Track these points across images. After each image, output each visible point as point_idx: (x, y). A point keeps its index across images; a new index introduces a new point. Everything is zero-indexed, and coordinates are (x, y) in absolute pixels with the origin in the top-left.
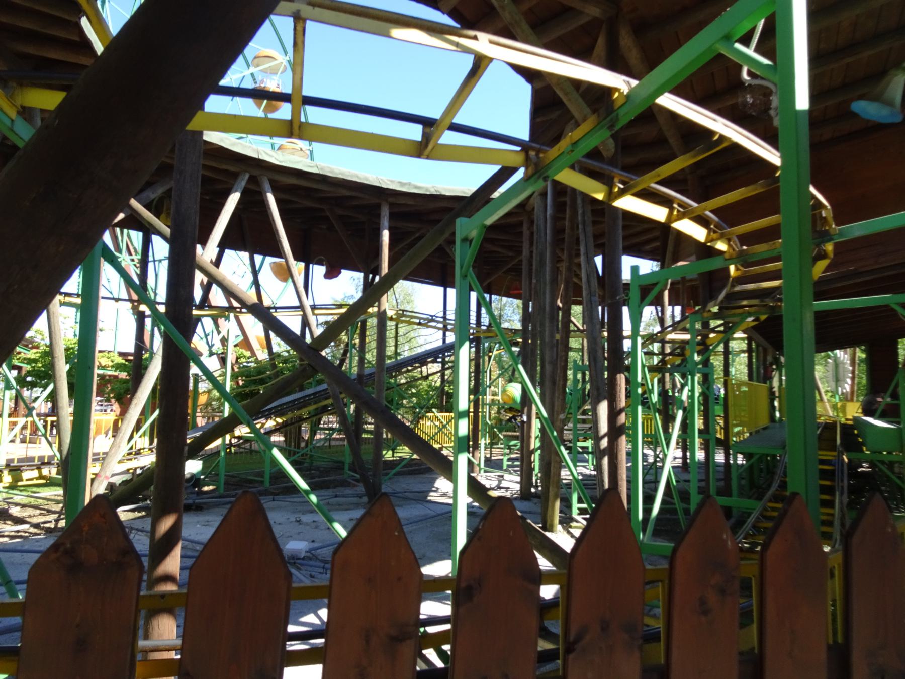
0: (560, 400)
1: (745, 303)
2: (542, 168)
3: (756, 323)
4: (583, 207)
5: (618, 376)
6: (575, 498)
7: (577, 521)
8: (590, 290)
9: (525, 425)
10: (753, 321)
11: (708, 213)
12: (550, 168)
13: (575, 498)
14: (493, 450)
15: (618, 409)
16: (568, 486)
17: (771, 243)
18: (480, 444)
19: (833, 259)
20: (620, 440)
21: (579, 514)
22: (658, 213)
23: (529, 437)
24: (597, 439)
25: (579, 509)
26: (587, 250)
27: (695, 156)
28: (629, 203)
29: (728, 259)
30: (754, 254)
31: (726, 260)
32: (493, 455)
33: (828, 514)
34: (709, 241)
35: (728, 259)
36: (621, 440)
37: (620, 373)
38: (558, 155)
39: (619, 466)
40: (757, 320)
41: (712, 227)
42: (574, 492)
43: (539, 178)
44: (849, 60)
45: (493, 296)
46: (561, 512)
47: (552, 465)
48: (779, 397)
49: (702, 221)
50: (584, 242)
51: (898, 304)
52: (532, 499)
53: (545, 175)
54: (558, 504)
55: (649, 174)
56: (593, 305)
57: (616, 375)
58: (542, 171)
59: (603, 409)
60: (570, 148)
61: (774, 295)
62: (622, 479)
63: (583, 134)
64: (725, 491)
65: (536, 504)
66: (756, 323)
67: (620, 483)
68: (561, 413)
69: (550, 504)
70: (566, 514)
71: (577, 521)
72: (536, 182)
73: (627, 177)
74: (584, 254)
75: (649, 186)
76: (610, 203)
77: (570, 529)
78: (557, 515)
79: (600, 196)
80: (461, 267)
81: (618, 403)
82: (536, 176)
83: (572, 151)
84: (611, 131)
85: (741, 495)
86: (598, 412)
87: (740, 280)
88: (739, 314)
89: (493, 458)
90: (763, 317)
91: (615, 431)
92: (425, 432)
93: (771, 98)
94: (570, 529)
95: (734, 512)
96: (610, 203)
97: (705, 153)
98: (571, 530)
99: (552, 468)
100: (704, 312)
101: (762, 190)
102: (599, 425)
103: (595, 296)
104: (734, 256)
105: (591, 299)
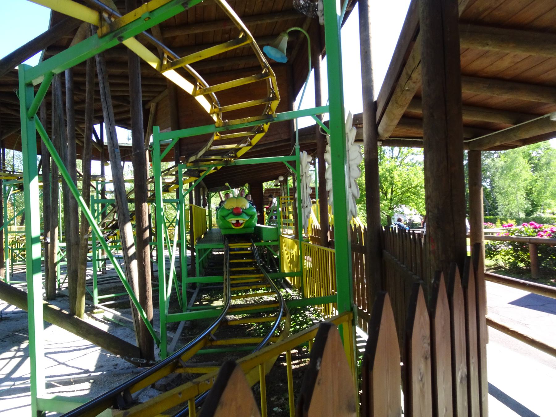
0: (84, 225)
1: (213, 157)
2: (118, 29)
3: (215, 171)
4: (103, 83)
5: (144, 204)
6: (96, 292)
7: (98, 308)
8: (113, 144)
9: (49, 245)
10: (214, 169)
11: (213, 93)
12: (126, 30)
13: (96, 292)
14: (14, 266)
15: (144, 227)
16: (90, 283)
17: (242, 119)
18: (5, 263)
19: (266, 133)
20: (146, 248)
21: (99, 303)
22: (187, 87)
23: (53, 253)
24: (126, 249)
25: (99, 300)
26: (108, 114)
27: (227, 47)
28: (171, 75)
29: (218, 127)
30: (232, 125)
31: (216, 127)
32: (14, 270)
33: (233, 279)
34: (212, 113)
35: (218, 127)
36: (147, 249)
37: (145, 202)
38: (134, 19)
39: (146, 268)
40: (216, 168)
41: (214, 103)
42: (95, 288)
43: (114, 36)
44: (259, 22)
45: (6, 149)
46: (86, 304)
47: (79, 272)
48: (206, 216)
49: (209, 98)
50: (106, 109)
51: (286, 161)
52: (56, 298)
53: (119, 35)
54: (84, 299)
55: (192, 54)
56: (116, 155)
57: (142, 204)
58: (117, 31)
59: (129, 230)
60: (147, 15)
61: (227, 154)
62: (148, 275)
63: (164, 3)
64: (191, 273)
65: (60, 301)
66: (215, 171)
67: (147, 278)
68: (85, 234)
69: (77, 300)
70: (89, 305)
71: (98, 308)
72: (111, 40)
73: (173, 55)
74: (107, 118)
75: (186, 66)
76: (161, 72)
77: (93, 315)
78: (83, 306)
79: (154, 65)
80: (28, 109)
81: (144, 223)
82: (111, 35)
83: (149, 18)
84: (185, 7)
85: (201, 274)
86: (125, 230)
87: (216, 143)
88: (208, 164)
89: (14, 273)
90: (219, 167)
91: (141, 243)
92: (308, 261)
93: (316, 4)
94: (93, 315)
95: (198, 285)
96: (161, 72)
97: (234, 45)
98: (94, 315)
99: (79, 274)
100: (187, 163)
101: (254, 81)
102: (126, 240)
103: (117, 148)
104: (221, 125)
105: (114, 150)
